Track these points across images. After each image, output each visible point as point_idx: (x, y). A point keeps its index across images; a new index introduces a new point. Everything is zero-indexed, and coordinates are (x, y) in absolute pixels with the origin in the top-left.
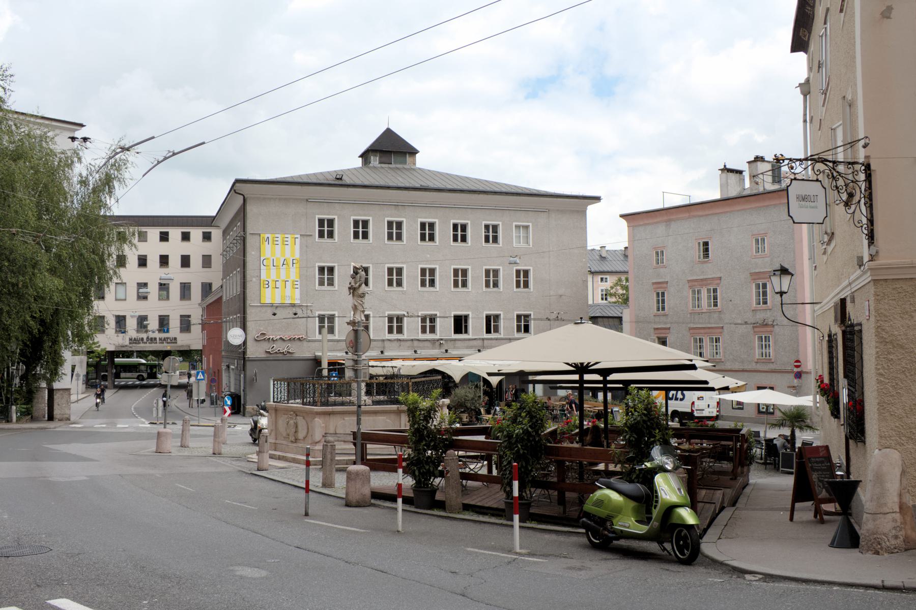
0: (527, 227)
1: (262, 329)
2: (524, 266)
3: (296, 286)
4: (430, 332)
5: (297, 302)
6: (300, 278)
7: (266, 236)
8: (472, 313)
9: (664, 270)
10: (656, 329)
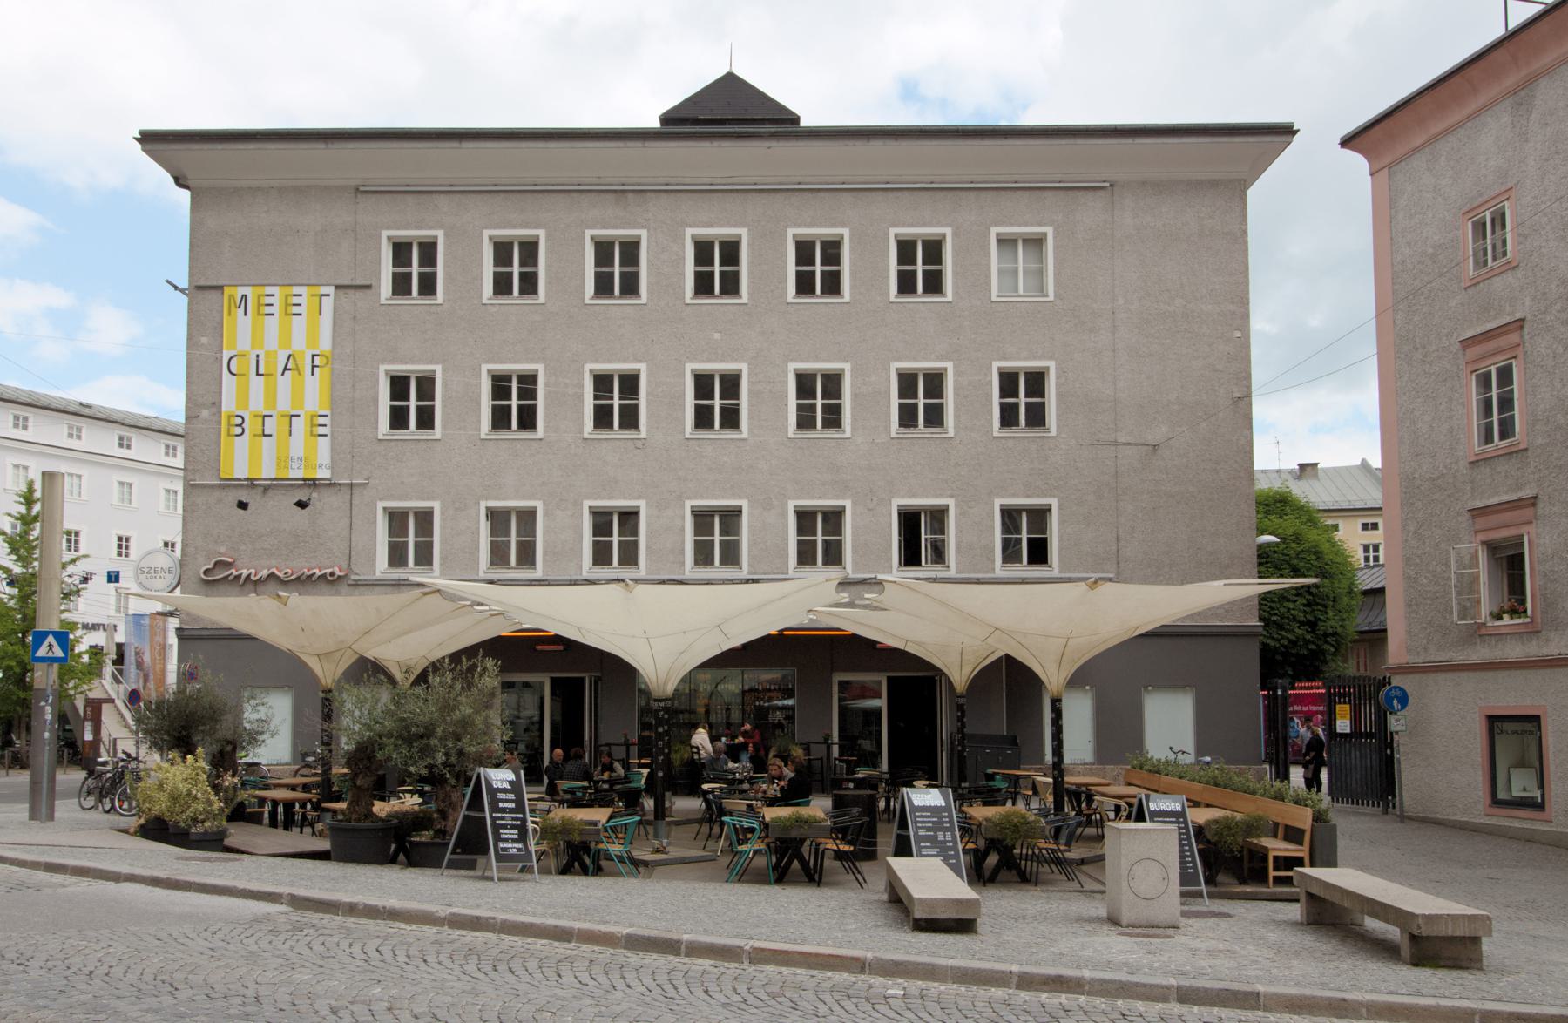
0: (1036, 242)
1: (223, 549)
2: (1026, 359)
3: (322, 430)
4: (724, 562)
5: (324, 474)
6: (332, 409)
7: (241, 291)
8: (854, 504)
9: (1509, 277)
10: (1477, 513)
